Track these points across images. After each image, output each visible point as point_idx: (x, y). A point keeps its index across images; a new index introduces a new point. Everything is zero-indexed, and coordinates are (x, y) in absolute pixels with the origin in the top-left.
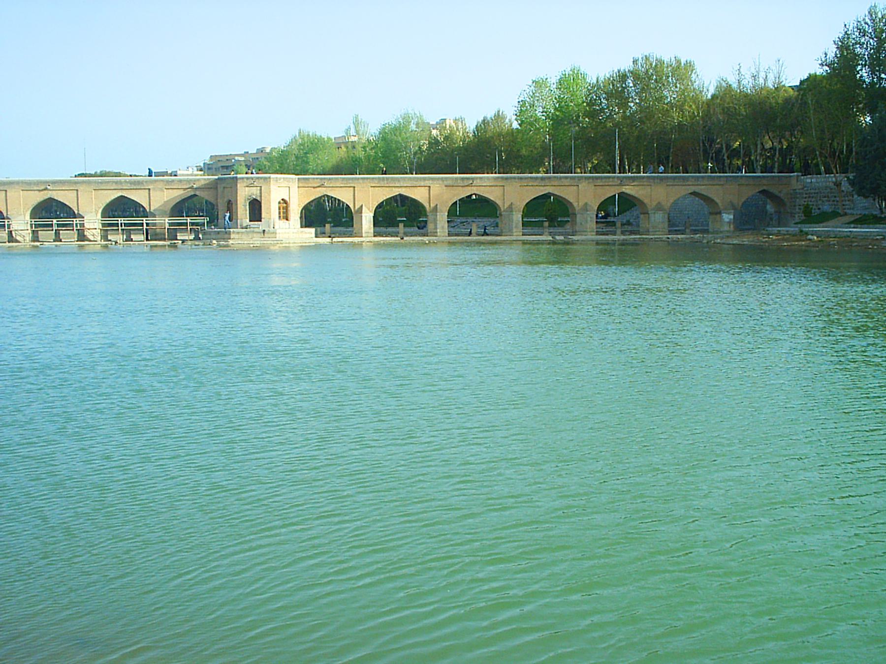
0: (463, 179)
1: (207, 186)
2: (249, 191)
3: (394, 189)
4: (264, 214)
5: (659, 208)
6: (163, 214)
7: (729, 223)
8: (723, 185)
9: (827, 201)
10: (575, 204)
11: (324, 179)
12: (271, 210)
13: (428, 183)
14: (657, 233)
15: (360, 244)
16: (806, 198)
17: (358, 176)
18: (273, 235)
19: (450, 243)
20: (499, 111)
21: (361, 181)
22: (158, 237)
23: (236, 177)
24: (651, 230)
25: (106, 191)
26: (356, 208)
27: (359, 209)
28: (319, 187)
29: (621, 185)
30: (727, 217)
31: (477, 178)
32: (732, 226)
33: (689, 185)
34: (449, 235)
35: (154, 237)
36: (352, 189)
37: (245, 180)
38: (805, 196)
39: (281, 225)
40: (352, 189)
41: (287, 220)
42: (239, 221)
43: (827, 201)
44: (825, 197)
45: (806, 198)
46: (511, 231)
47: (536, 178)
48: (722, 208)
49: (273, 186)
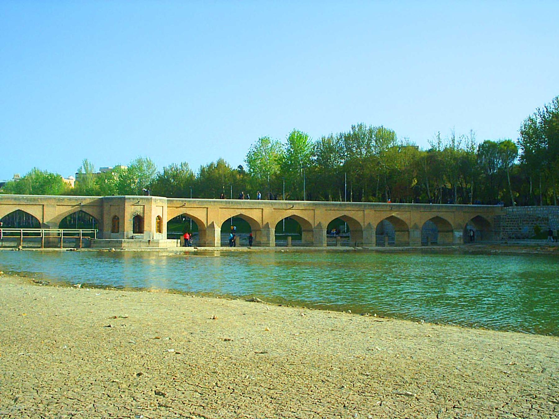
0: (286, 204)
1: (92, 205)
2: (134, 209)
3: (236, 210)
4: (146, 228)
5: (416, 227)
6: (54, 225)
7: (460, 238)
8: (454, 212)
9: (526, 223)
10: (362, 224)
11: (185, 201)
12: (150, 224)
13: (261, 206)
14: (416, 245)
15: (212, 252)
16: (508, 221)
17: (191, 199)
18: (155, 245)
19: (377, 251)
20: (35, 168)
21: (212, 203)
22: (51, 245)
23: (124, 198)
24: (411, 243)
25: (6, 206)
26: (208, 225)
27: (210, 225)
28: (180, 207)
29: (391, 210)
30: (458, 234)
31: (296, 204)
32: (462, 240)
33: (434, 212)
34: (276, 246)
35: (46, 245)
36: (205, 209)
37: (132, 200)
38: (507, 220)
39: (157, 236)
40: (205, 209)
41: (160, 232)
42: (125, 232)
43: (526, 223)
44: (525, 221)
45: (508, 221)
46: (322, 243)
47: (336, 205)
48: (453, 228)
49: (154, 205)
